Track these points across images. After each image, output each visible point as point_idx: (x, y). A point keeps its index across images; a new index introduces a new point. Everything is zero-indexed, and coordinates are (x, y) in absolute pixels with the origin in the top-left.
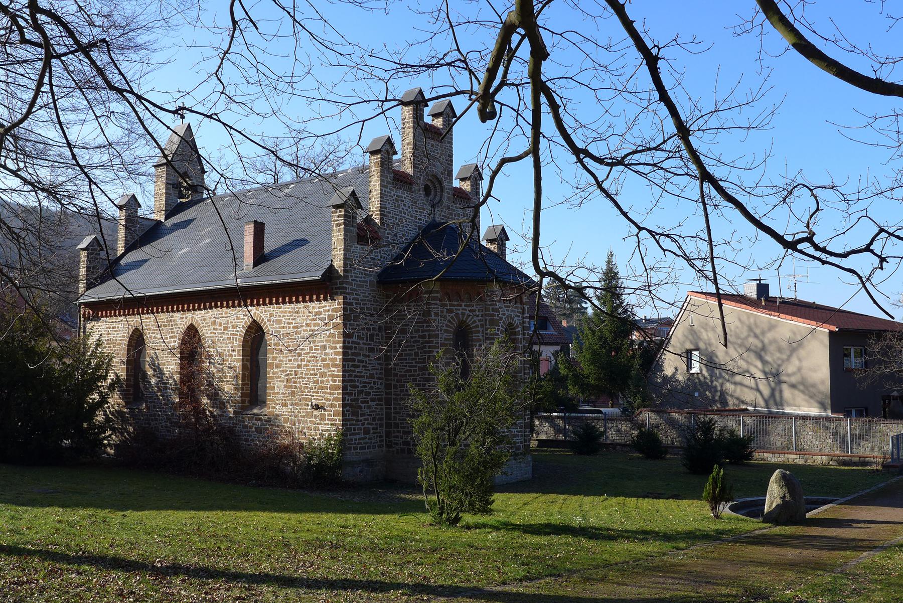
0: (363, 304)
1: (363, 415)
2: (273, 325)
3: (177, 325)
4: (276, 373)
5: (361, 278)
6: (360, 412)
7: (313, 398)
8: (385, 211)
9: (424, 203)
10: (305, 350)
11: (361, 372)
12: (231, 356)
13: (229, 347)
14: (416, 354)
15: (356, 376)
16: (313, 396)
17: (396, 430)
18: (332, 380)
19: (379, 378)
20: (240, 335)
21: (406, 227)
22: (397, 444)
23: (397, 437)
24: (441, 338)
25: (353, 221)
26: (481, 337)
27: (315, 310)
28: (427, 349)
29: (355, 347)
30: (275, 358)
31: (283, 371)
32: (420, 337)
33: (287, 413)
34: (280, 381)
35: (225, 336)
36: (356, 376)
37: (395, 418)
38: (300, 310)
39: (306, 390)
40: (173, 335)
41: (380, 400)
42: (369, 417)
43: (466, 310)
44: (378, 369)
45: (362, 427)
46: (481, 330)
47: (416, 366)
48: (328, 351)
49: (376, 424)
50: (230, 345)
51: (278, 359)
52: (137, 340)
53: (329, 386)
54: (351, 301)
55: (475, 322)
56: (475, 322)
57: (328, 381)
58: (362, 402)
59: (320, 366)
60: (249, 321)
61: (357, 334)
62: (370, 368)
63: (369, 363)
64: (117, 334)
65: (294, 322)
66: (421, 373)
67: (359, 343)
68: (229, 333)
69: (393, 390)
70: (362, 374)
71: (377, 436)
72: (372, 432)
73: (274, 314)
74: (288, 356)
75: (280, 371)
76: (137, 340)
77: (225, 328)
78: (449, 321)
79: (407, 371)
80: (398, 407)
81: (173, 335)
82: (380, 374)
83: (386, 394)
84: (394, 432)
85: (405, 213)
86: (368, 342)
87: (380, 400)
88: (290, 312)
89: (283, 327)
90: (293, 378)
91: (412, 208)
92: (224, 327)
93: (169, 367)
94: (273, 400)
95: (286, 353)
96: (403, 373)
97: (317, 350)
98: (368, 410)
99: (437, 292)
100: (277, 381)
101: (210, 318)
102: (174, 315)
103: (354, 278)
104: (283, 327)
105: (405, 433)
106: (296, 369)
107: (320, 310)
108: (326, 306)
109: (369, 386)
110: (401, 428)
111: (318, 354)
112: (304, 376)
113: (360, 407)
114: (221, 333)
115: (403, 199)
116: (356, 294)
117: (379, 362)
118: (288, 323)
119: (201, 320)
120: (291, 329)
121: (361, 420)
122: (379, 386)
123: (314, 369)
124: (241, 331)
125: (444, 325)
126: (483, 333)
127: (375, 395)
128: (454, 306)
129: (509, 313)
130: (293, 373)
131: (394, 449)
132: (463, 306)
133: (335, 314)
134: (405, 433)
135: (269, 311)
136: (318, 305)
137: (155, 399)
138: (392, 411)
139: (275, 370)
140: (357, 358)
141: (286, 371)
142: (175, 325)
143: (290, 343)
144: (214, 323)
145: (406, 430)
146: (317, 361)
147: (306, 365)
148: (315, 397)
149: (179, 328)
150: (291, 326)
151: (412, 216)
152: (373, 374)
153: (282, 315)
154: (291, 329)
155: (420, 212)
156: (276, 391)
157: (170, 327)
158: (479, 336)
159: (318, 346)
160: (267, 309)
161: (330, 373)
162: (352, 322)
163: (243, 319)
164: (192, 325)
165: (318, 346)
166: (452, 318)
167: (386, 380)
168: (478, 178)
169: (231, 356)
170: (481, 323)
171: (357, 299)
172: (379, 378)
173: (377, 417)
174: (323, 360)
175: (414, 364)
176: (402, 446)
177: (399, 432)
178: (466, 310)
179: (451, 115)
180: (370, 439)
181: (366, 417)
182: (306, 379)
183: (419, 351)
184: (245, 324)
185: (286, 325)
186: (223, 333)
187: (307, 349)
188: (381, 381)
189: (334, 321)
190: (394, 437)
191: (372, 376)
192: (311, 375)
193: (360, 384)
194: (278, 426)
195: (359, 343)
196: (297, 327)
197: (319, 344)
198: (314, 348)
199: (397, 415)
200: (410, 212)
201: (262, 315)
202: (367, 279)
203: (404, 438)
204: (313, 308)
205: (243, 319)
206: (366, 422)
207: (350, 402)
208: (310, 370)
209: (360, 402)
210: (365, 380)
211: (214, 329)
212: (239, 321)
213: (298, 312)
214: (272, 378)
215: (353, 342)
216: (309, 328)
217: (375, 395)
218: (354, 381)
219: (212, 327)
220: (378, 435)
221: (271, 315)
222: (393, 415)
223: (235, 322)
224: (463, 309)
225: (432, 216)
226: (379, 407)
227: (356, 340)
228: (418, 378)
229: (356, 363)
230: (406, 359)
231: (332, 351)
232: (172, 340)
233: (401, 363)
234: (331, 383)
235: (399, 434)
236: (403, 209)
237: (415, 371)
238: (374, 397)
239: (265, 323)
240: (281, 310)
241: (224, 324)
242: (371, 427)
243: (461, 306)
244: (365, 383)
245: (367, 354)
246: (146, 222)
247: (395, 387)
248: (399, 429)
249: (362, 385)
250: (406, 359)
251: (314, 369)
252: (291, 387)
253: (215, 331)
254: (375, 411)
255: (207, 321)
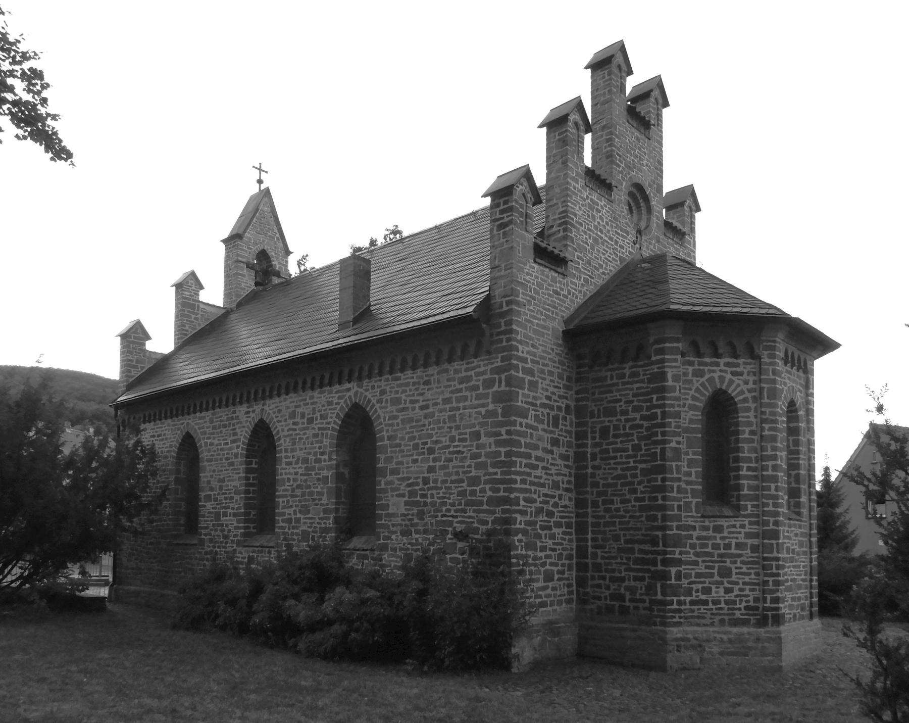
0: (544, 365)
1: (543, 549)
2: (386, 407)
3: (241, 423)
4: (391, 483)
5: (539, 319)
6: (539, 544)
7: (456, 520)
8: (575, 219)
9: (627, 224)
10: (441, 442)
11: (541, 477)
12: (318, 461)
13: (315, 448)
14: (636, 448)
15: (532, 483)
16: (456, 517)
17: (596, 574)
18: (490, 489)
19: (567, 490)
20: (333, 429)
21: (604, 254)
22: (599, 598)
23: (599, 586)
24: (685, 419)
25: (526, 223)
26: (752, 419)
27: (460, 375)
28: (660, 438)
29: (532, 434)
30: (389, 460)
31: (403, 479)
32: (643, 418)
33: (409, 546)
34: (398, 496)
35: (310, 433)
36: (532, 483)
37: (595, 555)
38: (432, 379)
39: (444, 509)
40: (235, 437)
41: (568, 525)
42: (553, 553)
43: (726, 372)
44: (565, 475)
45: (542, 569)
46: (753, 406)
47: (635, 468)
48: (483, 439)
49: (563, 565)
50: (317, 445)
51: (395, 460)
52: (188, 445)
53: (485, 499)
54: (525, 355)
55: (742, 392)
56: (742, 392)
57: (483, 491)
58: (543, 528)
59: (470, 466)
60: (347, 405)
61: (534, 413)
62: (553, 472)
63: (552, 464)
64: (164, 444)
65: (421, 398)
66: (645, 479)
67: (536, 429)
68: (316, 427)
69: (589, 510)
70: (542, 481)
71: (564, 584)
72: (556, 577)
73: (388, 390)
74: (412, 455)
75: (399, 479)
76: (188, 445)
77: (310, 421)
78: (697, 390)
79: (618, 477)
80: (600, 536)
81: (235, 437)
82: (569, 482)
83: (578, 515)
84: (593, 578)
85: (601, 232)
86: (551, 428)
87: (568, 525)
88: (414, 384)
89: (403, 409)
90: (420, 490)
91: (612, 226)
92: (308, 419)
93: (229, 483)
94: (386, 527)
95: (408, 451)
96: (610, 481)
97: (465, 440)
98: (550, 542)
99: (678, 340)
100: (392, 496)
101: (287, 408)
102: (237, 410)
103: (528, 318)
104: (403, 409)
105: (613, 580)
106: (426, 475)
107: (469, 373)
108: (479, 366)
109: (552, 501)
110: (607, 571)
111: (464, 447)
112: (439, 485)
113: (539, 536)
114: (304, 429)
115: (600, 208)
116: (533, 346)
117: (566, 463)
118: (412, 402)
119: (274, 413)
120: (417, 410)
121: (541, 558)
122: (567, 503)
123: (457, 473)
124: (334, 421)
125: (689, 397)
126: (756, 410)
127: (561, 517)
128: (706, 364)
129: (791, 384)
130: (420, 480)
131: (593, 607)
132: (722, 365)
133: (497, 376)
134: (613, 580)
135: (379, 387)
136: (465, 366)
137: (212, 530)
138: (589, 543)
139: (389, 478)
140: (534, 453)
141: (409, 478)
142: (238, 423)
143: (415, 434)
144: (293, 415)
145: (617, 575)
146: (463, 459)
147: (443, 467)
148: (459, 519)
149: (244, 427)
150: (417, 405)
151: (611, 239)
152: (559, 481)
153: (400, 389)
154: (417, 410)
155: (622, 236)
156: (390, 511)
157: (232, 428)
158: (748, 417)
159: (466, 434)
160: (376, 384)
161: (487, 477)
162: (526, 391)
163: (338, 404)
164: (262, 421)
165: (466, 434)
166: (703, 385)
167: (578, 493)
168: (693, 208)
169: (318, 461)
170: (754, 394)
171: (534, 355)
172: (567, 490)
173: (565, 553)
174: (474, 456)
175: (632, 464)
176: (608, 602)
177: (604, 578)
178: (726, 372)
179: (660, 101)
180: (554, 589)
181: (548, 552)
182: (443, 490)
183: (643, 443)
184: (340, 410)
185: (408, 405)
186: (307, 428)
187: (445, 441)
188: (569, 495)
189: (496, 388)
190: (593, 586)
191: (556, 485)
192: (452, 482)
193: (539, 497)
194: (257, 589)
195: (536, 429)
196: (426, 407)
197: (468, 431)
198: (457, 437)
199: (599, 551)
200: (608, 231)
201: (367, 394)
202: (549, 324)
203: (612, 587)
204: (456, 372)
205: (338, 404)
206: (548, 561)
207: (523, 526)
208: (450, 474)
209: (538, 527)
210: (545, 491)
211: (294, 424)
212: (330, 407)
213: (427, 383)
214: (385, 491)
215: (528, 426)
216: (448, 406)
217: (561, 517)
218: (529, 491)
219: (290, 422)
220: (566, 582)
221: (383, 392)
222: (590, 549)
223: (325, 410)
224: (721, 371)
225: (637, 246)
226: (567, 537)
227: (533, 423)
228: (641, 488)
229: (533, 461)
230: (615, 458)
231: (492, 440)
232: (235, 445)
233: (606, 464)
234: (489, 493)
235: (601, 582)
236: (599, 223)
237: (635, 476)
238: (559, 519)
239: (373, 405)
240: (399, 382)
241: (309, 414)
242: (555, 569)
243: (718, 365)
244: (545, 495)
245: (549, 447)
246: (212, 310)
247: (595, 504)
248: (604, 574)
249: (542, 498)
250: (615, 458)
251: (457, 473)
252: (417, 504)
253: (294, 427)
254: (561, 544)
255: (284, 412)
